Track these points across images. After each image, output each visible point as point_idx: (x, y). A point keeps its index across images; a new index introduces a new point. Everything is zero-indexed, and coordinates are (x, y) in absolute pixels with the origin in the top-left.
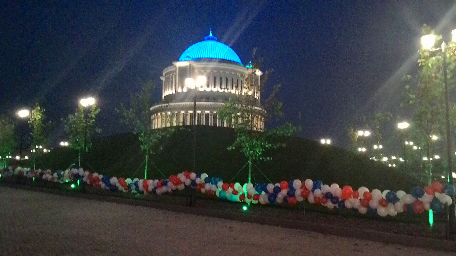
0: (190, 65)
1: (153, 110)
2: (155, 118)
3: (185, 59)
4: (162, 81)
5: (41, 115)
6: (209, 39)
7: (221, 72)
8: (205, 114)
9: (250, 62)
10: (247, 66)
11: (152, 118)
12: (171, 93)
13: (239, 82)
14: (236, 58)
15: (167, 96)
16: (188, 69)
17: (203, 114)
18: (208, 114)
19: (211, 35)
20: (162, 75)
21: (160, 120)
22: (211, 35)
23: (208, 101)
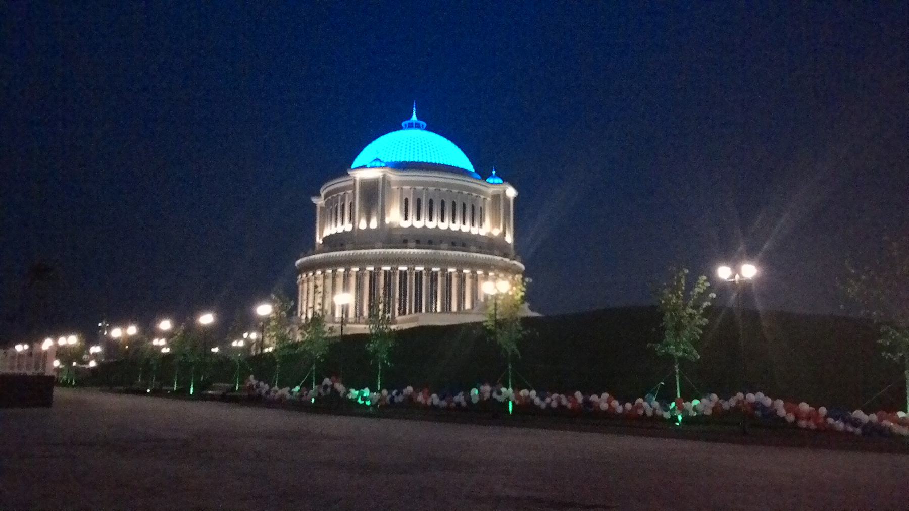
0: (384, 175)
2: (308, 281)
3: (373, 164)
5: (524, 289)
6: (410, 126)
7: (432, 189)
8: (398, 272)
9: (494, 172)
10: (490, 180)
14: (468, 166)
16: (381, 185)
17: (411, 273)
18: (421, 272)
19: (414, 118)
22: (414, 118)
23: (480, 252)
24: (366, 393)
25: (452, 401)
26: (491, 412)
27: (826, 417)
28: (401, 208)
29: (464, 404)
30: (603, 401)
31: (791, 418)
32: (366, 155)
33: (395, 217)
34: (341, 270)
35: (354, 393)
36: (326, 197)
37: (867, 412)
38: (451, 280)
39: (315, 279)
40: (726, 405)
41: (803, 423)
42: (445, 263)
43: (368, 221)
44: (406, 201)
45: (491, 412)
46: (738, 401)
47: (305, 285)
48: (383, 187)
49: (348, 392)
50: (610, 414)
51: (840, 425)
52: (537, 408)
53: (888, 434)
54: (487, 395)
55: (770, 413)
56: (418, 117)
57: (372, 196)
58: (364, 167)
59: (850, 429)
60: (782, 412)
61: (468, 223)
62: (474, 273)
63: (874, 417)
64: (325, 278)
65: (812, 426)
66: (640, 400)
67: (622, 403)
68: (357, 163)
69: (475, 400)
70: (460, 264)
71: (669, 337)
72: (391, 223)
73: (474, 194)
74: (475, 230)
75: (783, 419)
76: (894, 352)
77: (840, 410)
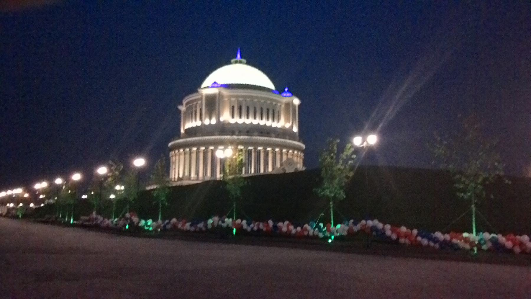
0: (220, 92)
1: (172, 145)
2: (176, 155)
3: (214, 85)
4: (179, 111)
6: (236, 62)
9: (286, 90)
11: (170, 156)
12: (194, 126)
13: (275, 111)
14: (272, 87)
15: (189, 129)
16: (218, 97)
20: (182, 104)
21: (182, 157)
24: (150, 222)
25: (196, 228)
26: (221, 235)
27: (417, 236)
28: (230, 112)
29: (204, 229)
30: (284, 226)
31: (394, 237)
32: (208, 81)
33: (226, 117)
34: (195, 149)
35: (143, 222)
36: (187, 104)
37: (443, 233)
38: (260, 154)
39: (180, 154)
40: (356, 228)
41: (402, 240)
42: (256, 144)
43: (210, 119)
44: (233, 107)
45: (221, 235)
46: (363, 226)
47: (177, 157)
48: (219, 99)
49: (139, 222)
50: (288, 235)
51: (425, 242)
52: (246, 230)
53: (455, 248)
54: (216, 224)
55: (382, 233)
56: (241, 57)
57: (212, 104)
58: (208, 87)
59: (432, 244)
60: (388, 233)
61: (270, 120)
62: (281, 151)
63: (447, 237)
64: (185, 154)
65: (408, 242)
66: (306, 226)
67: (295, 227)
68: (203, 85)
69: (210, 226)
70: (265, 145)
71: (326, 184)
72: (224, 121)
73: (274, 103)
74: (275, 125)
75: (389, 237)
76: (465, 193)
77: (426, 232)
